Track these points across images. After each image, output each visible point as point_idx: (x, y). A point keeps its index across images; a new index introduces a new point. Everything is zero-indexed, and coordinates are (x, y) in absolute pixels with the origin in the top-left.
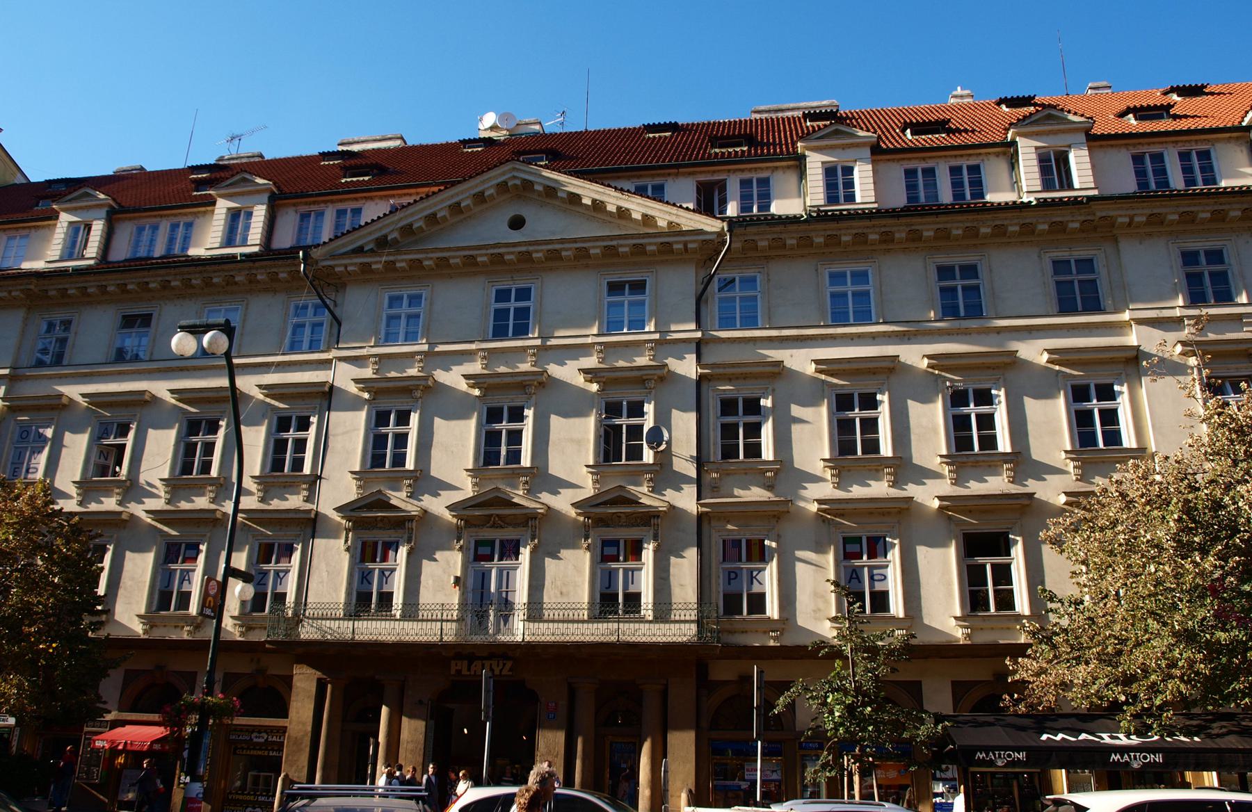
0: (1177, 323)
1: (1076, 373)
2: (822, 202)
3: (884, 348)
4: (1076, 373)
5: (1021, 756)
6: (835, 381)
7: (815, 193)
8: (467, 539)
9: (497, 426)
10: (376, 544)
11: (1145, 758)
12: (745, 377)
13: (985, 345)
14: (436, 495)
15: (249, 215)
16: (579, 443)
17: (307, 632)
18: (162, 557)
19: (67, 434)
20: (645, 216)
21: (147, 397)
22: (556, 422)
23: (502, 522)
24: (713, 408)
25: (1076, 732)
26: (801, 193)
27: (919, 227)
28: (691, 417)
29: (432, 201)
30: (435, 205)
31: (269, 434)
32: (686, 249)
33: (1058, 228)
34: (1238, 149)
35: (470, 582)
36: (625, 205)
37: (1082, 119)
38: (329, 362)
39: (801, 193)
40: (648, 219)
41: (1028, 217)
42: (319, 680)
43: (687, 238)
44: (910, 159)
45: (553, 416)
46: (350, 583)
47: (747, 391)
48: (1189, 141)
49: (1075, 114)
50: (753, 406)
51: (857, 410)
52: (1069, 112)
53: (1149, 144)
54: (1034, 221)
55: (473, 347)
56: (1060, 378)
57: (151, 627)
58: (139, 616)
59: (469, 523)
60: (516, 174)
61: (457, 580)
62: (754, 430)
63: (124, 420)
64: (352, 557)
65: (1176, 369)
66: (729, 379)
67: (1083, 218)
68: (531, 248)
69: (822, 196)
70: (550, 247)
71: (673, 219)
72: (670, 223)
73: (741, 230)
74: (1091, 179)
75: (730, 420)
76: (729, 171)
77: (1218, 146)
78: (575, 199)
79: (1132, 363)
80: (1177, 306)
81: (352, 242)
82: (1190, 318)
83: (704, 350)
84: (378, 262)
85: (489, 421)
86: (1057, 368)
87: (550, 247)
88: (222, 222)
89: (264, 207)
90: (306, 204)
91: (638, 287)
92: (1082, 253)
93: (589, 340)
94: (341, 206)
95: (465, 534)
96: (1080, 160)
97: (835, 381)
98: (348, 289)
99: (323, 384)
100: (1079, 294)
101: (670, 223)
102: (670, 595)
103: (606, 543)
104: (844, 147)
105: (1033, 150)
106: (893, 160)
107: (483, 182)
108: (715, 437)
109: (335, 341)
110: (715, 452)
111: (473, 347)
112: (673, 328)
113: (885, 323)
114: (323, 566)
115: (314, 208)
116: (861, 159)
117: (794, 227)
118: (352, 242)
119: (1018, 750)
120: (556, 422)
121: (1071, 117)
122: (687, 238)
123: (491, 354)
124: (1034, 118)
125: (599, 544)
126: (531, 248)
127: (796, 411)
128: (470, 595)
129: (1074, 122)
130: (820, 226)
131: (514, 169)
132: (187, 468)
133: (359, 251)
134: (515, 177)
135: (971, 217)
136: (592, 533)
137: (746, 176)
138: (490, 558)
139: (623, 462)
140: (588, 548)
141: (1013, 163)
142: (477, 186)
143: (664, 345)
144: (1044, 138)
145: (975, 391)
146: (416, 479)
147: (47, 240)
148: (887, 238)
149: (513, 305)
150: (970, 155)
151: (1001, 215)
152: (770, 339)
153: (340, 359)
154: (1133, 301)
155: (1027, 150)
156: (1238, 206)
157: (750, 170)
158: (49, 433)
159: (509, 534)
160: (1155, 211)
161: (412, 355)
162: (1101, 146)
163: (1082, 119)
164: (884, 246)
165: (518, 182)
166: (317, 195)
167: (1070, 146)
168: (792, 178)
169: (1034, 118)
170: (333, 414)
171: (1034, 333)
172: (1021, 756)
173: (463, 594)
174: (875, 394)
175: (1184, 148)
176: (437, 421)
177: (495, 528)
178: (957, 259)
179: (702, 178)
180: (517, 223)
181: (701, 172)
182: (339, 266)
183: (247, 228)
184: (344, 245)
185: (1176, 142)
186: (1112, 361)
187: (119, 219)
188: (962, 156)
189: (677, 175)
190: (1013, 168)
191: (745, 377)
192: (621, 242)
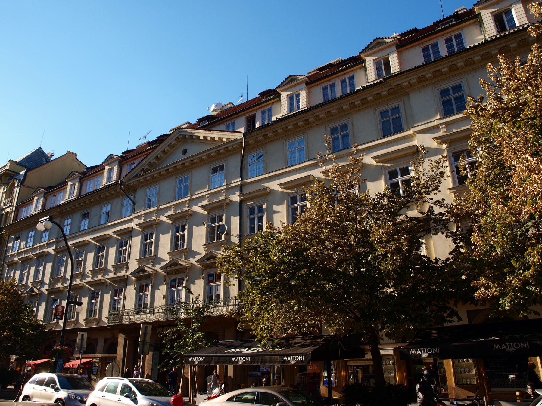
0: (437, 128)
1: (389, 165)
2: (495, 34)
3: (309, 172)
4: (389, 165)
5: (203, 359)
6: (290, 191)
7: (490, 30)
8: (168, 280)
9: (396, 180)
10: (143, 285)
11: (297, 358)
12: (257, 197)
13: (347, 161)
14: (194, 257)
15: (298, 95)
16: (201, 236)
17: (125, 321)
18: (138, 291)
19: (194, 227)
20: (219, 138)
21: (86, 242)
22: (195, 228)
23: (178, 271)
24: (246, 211)
25: (236, 348)
26: (482, 32)
27: (317, 114)
28: (238, 218)
29: (155, 151)
30: (156, 153)
31: (288, 206)
32: (410, 85)
33: (378, 97)
34: (474, 28)
35: (169, 298)
36: (213, 136)
37: (392, 40)
38: (132, 219)
39: (482, 32)
40: (221, 139)
41: (375, 91)
42: (125, 339)
43: (232, 144)
44: (324, 82)
45: (194, 227)
46: (136, 301)
47: (257, 202)
48: (450, 32)
49: (388, 38)
50: (261, 210)
51: (399, 177)
52: (386, 38)
53: (429, 40)
54: (365, 97)
55: (170, 205)
56: (383, 169)
57: (87, 323)
58: (84, 320)
59: (168, 273)
60: (180, 133)
61: (164, 296)
62: (260, 219)
63: (152, 232)
64: (136, 291)
65: (436, 152)
66: (251, 199)
67: (387, 89)
68: (184, 162)
69: (495, 30)
70: (189, 160)
71: (228, 137)
72: (227, 139)
73: (249, 135)
74: (526, 18)
75: (252, 216)
76: (257, 109)
77: (464, 30)
78: (198, 137)
79: (416, 153)
80: (437, 120)
81: (133, 174)
82: (442, 124)
83: (244, 189)
84: (148, 176)
85: (292, 203)
86: (381, 164)
87: (189, 160)
88: (286, 105)
89: (305, 92)
90: (130, 161)
91: (222, 168)
92: (393, 105)
93: (204, 194)
94: (342, 78)
95: (167, 279)
96: (518, 10)
97: (290, 191)
98: (138, 191)
99: (129, 228)
100: (392, 125)
101: (227, 139)
102: (229, 294)
103: (172, 281)
104: (295, 86)
105: (372, 61)
106: (317, 85)
107: (170, 140)
108: (247, 225)
109: (133, 212)
110: (247, 231)
111: (170, 205)
112: (232, 182)
113: (309, 161)
114: (129, 296)
115: (266, 108)
116: (301, 89)
117: (269, 128)
118: (133, 174)
119: (202, 357)
120: (195, 228)
121: (387, 40)
122: (232, 144)
123: (447, 124)
124: (371, 46)
125: (207, 276)
126: (184, 162)
127: (276, 208)
128: (169, 302)
129: (388, 42)
130: (279, 125)
131: (179, 132)
132: (176, 247)
133: (136, 176)
134: (180, 135)
135: (337, 103)
136: (204, 272)
137: (342, 78)
138: (174, 287)
139: (216, 241)
140: (203, 278)
141: (481, 24)
142: (168, 142)
143: (229, 190)
144: (377, 54)
145: (401, 169)
146: (154, 259)
147: (102, 178)
148: (307, 123)
149: (391, 118)
150: (348, 72)
151: (285, 122)
152: (266, 178)
153: (135, 217)
154: (416, 123)
155: (487, 16)
156: (461, 60)
157: (264, 107)
158: (65, 259)
159: (180, 276)
160: (419, 75)
161: (152, 212)
162: (407, 49)
163: (392, 40)
164: (308, 126)
165: (181, 136)
166: (131, 157)
167: (511, 5)
168: (362, 72)
169: (371, 46)
170: (133, 238)
171: (371, 150)
172: (203, 359)
173: (166, 302)
174: (408, 167)
175: (447, 37)
176: (161, 235)
177: (176, 274)
178: (449, 84)
179: (248, 115)
180: (185, 152)
181: (247, 113)
182: (134, 182)
183: (298, 102)
184: (132, 175)
185: (443, 35)
186: (406, 155)
187: (123, 164)
188: (345, 74)
189: (239, 116)
190: (481, 27)
191: (257, 197)
192: (211, 151)
